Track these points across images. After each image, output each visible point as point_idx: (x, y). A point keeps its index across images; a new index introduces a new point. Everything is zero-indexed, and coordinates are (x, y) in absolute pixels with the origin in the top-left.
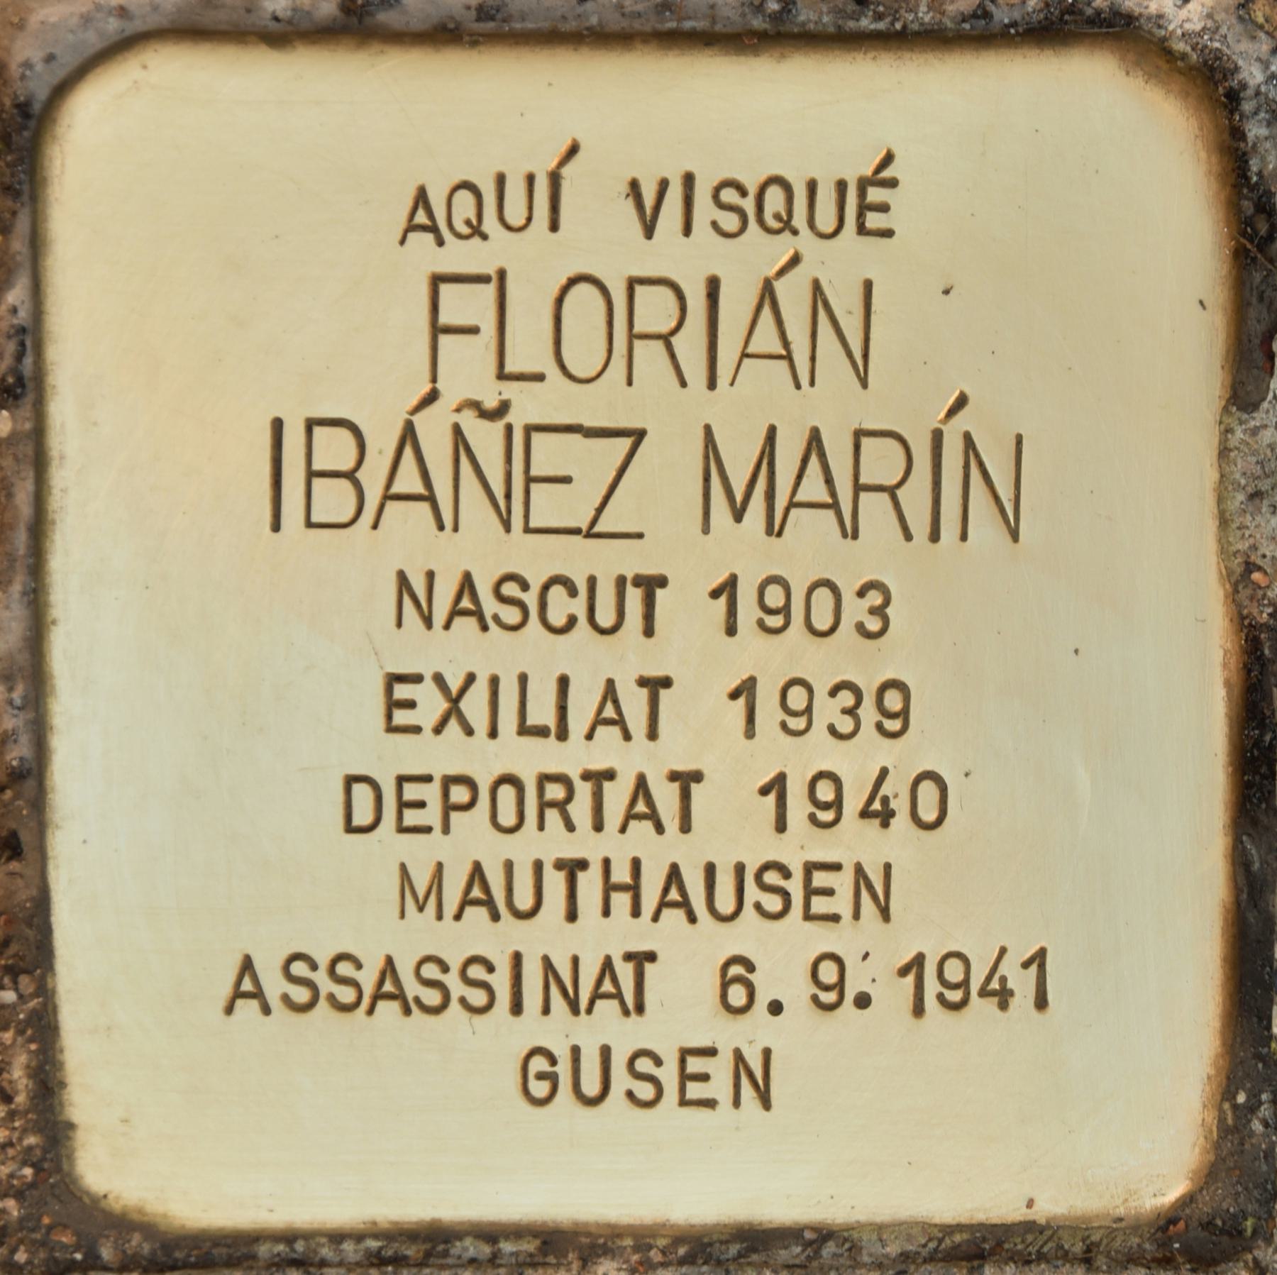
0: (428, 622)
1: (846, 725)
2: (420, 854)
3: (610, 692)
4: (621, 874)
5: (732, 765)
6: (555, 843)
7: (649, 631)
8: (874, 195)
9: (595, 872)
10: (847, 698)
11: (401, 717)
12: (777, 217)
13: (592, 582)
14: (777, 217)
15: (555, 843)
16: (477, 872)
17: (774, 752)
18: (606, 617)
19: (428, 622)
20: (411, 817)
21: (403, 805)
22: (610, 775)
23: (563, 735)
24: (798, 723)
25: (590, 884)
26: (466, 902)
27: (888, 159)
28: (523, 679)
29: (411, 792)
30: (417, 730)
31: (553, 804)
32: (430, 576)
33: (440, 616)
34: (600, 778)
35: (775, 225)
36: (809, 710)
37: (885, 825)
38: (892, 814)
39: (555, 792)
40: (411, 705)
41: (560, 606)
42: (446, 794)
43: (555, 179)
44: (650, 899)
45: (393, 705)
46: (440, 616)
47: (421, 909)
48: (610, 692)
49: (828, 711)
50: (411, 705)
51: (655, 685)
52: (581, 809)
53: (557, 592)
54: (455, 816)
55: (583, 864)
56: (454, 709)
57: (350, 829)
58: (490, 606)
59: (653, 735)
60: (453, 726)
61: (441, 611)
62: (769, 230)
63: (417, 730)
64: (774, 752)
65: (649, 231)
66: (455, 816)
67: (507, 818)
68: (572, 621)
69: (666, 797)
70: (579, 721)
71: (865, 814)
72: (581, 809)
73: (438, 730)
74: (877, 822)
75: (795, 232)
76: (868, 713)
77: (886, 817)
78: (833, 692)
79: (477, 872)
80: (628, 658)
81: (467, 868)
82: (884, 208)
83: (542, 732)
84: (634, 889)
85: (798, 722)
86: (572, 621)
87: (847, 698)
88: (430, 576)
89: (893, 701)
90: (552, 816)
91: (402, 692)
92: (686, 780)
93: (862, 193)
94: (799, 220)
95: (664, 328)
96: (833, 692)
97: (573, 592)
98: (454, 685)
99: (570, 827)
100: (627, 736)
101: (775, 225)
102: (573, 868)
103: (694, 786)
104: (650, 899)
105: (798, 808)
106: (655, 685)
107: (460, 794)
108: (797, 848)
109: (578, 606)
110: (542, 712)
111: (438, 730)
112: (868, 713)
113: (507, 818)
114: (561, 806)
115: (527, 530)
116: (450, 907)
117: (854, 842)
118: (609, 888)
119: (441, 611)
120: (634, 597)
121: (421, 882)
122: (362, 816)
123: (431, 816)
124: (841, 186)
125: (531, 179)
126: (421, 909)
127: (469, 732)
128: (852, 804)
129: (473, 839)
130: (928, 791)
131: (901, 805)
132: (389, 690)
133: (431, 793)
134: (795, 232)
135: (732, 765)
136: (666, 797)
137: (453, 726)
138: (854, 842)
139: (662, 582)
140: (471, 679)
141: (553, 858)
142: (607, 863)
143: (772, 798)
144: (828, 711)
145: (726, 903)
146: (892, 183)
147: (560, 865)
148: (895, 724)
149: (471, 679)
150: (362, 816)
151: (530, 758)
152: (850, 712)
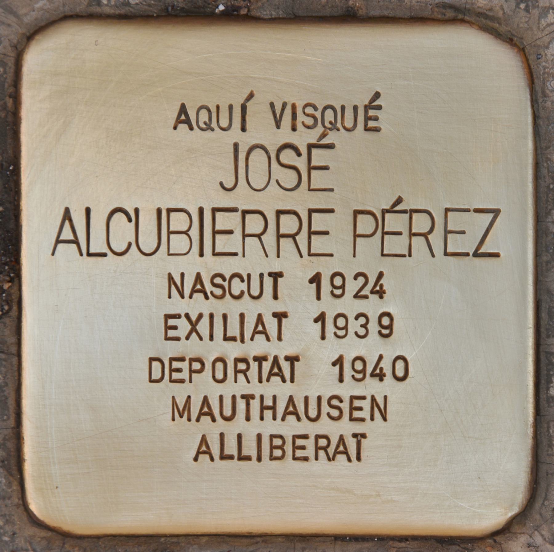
0: (182, 297)
1: (362, 332)
2: (181, 393)
4: (269, 402)
6: (241, 387)
8: (371, 113)
10: (362, 320)
11: (171, 333)
12: (205, 123)
13: (249, 276)
14: (331, 123)
15: (241, 387)
17: (333, 348)
20: (175, 376)
21: (172, 370)
22: (265, 359)
23: (242, 341)
24: (341, 333)
25: (255, 404)
26: (201, 414)
27: (377, 95)
28: (225, 317)
30: (178, 339)
31: (241, 371)
32: (182, 275)
33: (187, 292)
34: (260, 360)
35: (204, 126)
37: (381, 380)
38: (384, 375)
40: (175, 328)
41: (237, 287)
42: (190, 365)
43: (244, 108)
45: (168, 328)
46: (187, 292)
47: (181, 417)
49: (355, 326)
50: (175, 328)
51: (280, 316)
53: (236, 280)
54: (194, 375)
55: (253, 397)
56: (194, 329)
58: (209, 288)
59: (280, 338)
61: (187, 291)
62: (202, 129)
63: (178, 339)
67: (220, 375)
68: (242, 293)
70: (248, 334)
73: (187, 338)
74: (378, 378)
75: (213, 130)
76: (373, 327)
77: (381, 377)
78: (357, 318)
79: (206, 400)
80: (267, 306)
82: (376, 119)
83: (234, 339)
84: (273, 408)
85: (342, 332)
87: (362, 320)
88: (182, 275)
89: (386, 321)
90: (241, 376)
91: (171, 322)
92: (292, 360)
93: (366, 112)
94: (214, 124)
96: (357, 318)
97: (243, 281)
98: (194, 318)
100: (268, 339)
101: (204, 126)
102: (248, 398)
103: (296, 363)
106: (280, 316)
107: (196, 366)
108: (347, 390)
110: (234, 330)
111: (187, 338)
112: (373, 327)
114: (244, 372)
115: (215, 254)
116: (194, 416)
117: (371, 387)
118: (263, 408)
119: (187, 291)
120: (268, 282)
122: (156, 375)
123: (185, 375)
124: (356, 108)
125: (231, 107)
126: (181, 417)
127: (201, 339)
128: (369, 370)
129: (204, 386)
130: (400, 365)
131: (388, 370)
132: (166, 322)
133: (184, 365)
134: (213, 130)
140: (200, 316)
141: (240, 394)
142: (262, 397)
143: (337, 367)
144: (355, 326)
145: (313, 413)
146: (379, 108)
147: (243, 397)
148: (387, 331)
149: (200, 316)
150: (156, 375)
151: (233, 351)
152: (364, 326)
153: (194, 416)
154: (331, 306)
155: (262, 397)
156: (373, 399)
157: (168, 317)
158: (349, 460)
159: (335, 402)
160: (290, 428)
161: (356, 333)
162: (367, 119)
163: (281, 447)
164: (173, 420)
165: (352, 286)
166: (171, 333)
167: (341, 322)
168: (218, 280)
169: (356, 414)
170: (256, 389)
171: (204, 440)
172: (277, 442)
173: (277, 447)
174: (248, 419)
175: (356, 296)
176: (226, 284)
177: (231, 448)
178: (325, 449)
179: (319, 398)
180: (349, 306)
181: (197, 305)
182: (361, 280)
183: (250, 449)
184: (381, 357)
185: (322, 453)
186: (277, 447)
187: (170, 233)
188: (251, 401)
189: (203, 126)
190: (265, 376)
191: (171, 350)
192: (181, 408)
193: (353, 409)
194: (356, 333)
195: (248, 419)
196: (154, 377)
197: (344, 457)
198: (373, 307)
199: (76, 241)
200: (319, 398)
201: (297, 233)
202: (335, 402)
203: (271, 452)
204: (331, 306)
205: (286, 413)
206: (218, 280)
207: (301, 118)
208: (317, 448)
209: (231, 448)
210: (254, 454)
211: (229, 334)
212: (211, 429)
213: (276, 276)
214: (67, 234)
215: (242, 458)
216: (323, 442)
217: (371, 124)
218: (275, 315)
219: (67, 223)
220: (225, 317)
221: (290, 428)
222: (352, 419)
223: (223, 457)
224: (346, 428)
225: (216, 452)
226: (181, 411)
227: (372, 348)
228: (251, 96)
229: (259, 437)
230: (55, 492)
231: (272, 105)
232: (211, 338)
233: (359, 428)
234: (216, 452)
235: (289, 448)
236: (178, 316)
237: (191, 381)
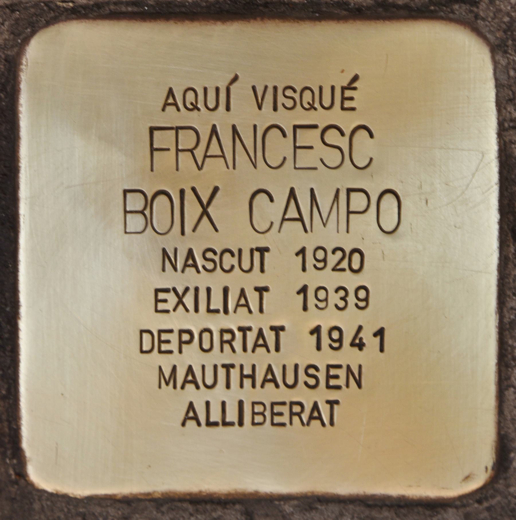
0: (175, 269)
1: (341, 304)
2: (166, 363)
3: (242, 293)
4: (247, 371)
5: (298, 325)
7: (262, 270)
9: (238, 368)
10: (342, 293)
11: (161, 306)
12: (192, 104)
13: (240, 251)
16: (190, 370)
18: (246, 266)
19: (175, 269)
21: (160, 342)
23: (226, 311)
24: (322, 305)
25: (235, 374)
26: (186, 382)
28: (209, 290)
29: (164, 337)
34: (243, 330)
35: (190, 107)
36: (326, 300)
39: (227, 337)
40: (165, 301)
41: (228, 261)
44: (259, 379)
45: (157, 301)
46: (179, 266)
48: (242, 293)
49: (335, 298)
50: (165, 301)
51: (261, 290)
52: (238, 344)
53: (227, 255)
54: (184, 346)
55: (233, 366)
56: (180, 302)
57: (142, 352)
58: (200, 262)
60: (181, 307)
63: (167, 311)
64: (315, 318)
65: (260, 108)
66: (184, 346)
67: (206, 346)
68: (233, 267)
69: (270, 337)
70: (231, 306)
71: (352, 344)
72: (238, 344)
73: (174, 310)
75: (315, 109)
76: (351, 299)
77: (361, 346)
78: (337, 291)
81: (265, 367)
82: (351, 99)
84: (252, 377)
86: (233, 267)
87: (342, 293)
88: (176, 250)
89: (362, 294)
90: (226, 347)
92: (277, 330)
94: (317, 105)
95: (190, 147)
96: (337, 291)
97: (233, 255)
99: (234, 351)
101: (190, 107)
102: (228, 367)
104: (259, 379)
105: (325, 341)
106: (261, 290)
108: (325, 358)
109: (235, 261)
110: (217, 303)
111: (174, 310)
113: (206, 346)
114: (229, 342)
116: (179, 384)
117: (348, 356)
118: (243, 376)
120: (257, 255)
121: (167, 373)
123: (174, 346)
126: (167, 384)
127: (187, 310)
128: (347, 340)
129: (192, 356)
132: (156, 296)
135: (298, 325)
136: (270, 337)
137: (181, 307)
138: (348, 356)
139: (267, 250)
140: (187, 289)
142: (242, 367)
147: (223, 366)
149: (187, 289)
151: (216, 324)
152: (343, 299)
153: (179, 384)
154: (314, 279)
155: (242, 367)
156: (348, 367)
157: (157, 291)
158: (323, 424)
159: (312, 371)
160: (269, 394)
161: (336, 306)
162: (344, 99)
163: (263, 414)
164: (160, 387)
165: (333, 259)
166: (161, 306)
167: (322, 294)
168: (209, 255)
169: (332, 382)
170: (239, 358)
171: (191, 406)
172: (258, 409)
173: (258, 414)
174: (228, 386)
175: (334, 269)
176: (217, 258)
177: (216, 416)
178: (299, 415)
179: (296, 366)
180: (330, 279)
181: (191, 278)
182: (339, 254)
183: (232, 416)
184: (360, 328)
185: (296, 419)
186: (258, 414)
187: (349, 212)
188: (232, 370)
189: (307, 106)
190: (250, 345)
191: (157, 322)
192: (167, 377)
193: (329, 377)
194: (336, 306)
195: (228, 386)
196: (145, 348)
197: (318, 422)
198: (351, 281)
199: (301, 219)
200: (296, 366)
201: (145, 208)
202: (312, 371)
203: (253, 419)
204: (314, 279)
205: (265, 381)
206: (209, 255)
207: (281, 99)
208: (292, 414)
209: (216, 416)
210: (236, 420)
211: (212, 307)
212: (198, 397)
213: (263, 250)
214: (292, 213)
215: (225, 424)
216: (296, 409)
217: (348, 104)
218: (257, 289)
219: (292, 202)
220: (209, 290)
221: (269, 394)
222: (328, 387)
223: (209, 424)
224: (321, 396)
225: (202, 418)
226: (168, 379)
227: (348, 321)
228: (235, 79)
229: (241, 403)
230: (55, 457)
231: (254, 88)
232: (197, 310)
233: (333, 395)
234: (202, 418)
235: (268, 413)
236: (167, 291)
237: (180, 352)
